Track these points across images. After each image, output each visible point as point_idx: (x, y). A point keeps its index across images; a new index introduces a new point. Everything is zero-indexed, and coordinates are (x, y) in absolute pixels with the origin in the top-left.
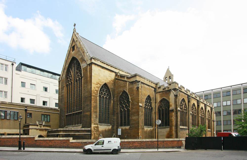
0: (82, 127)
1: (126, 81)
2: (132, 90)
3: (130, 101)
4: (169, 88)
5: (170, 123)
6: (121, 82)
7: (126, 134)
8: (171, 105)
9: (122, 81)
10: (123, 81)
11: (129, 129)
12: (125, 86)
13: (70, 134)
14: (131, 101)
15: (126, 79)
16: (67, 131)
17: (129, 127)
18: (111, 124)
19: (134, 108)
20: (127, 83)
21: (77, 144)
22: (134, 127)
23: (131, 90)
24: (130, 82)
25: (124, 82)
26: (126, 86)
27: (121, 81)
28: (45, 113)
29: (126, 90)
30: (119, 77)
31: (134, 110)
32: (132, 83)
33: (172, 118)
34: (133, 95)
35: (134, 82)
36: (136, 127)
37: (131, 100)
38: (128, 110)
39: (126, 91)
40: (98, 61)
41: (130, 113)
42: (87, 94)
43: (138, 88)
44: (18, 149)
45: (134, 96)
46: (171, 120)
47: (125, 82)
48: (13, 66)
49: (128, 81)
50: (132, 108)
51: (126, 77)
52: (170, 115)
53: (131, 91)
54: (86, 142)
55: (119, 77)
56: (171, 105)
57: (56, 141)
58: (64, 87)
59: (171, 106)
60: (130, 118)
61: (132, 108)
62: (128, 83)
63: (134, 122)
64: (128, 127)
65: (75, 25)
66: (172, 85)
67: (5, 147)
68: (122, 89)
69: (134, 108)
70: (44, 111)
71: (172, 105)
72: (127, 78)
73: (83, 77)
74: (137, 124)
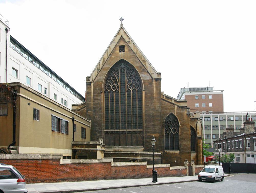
0: (144, 151)
1: (174, 104)
2: (181, 115)
3: (180, 125)
4: (194, 116)
5: (198, 149)
6: (168, 103)
7: (175, 159)
8: (199, 133)
9: (169, 103)
10: (170, 102)
11: (179, 153)
12: (173, 109)
13: (146, 159)
14: (181, 126)
15: (173, 102)
16: (144, 155)
17: (179, 151)
18: (143, 146)
19: (184, 133)
20: (175, 106)
21: (174, 172)
22: (185, 152)
23: (181, 115)
24: (178, 106)
25: (171, 104)
26: (174, 109)
27: (167, 103)
28: (83, 125)
29: (175, 113)
30: (165, 97)
31: (184, 135)
32: (182, 108)
33: (200, 145)
34: (183, 120)
35: (184, 108)
36: (187, 152)
37: (180, 125)
38: (178, 135)
39: (174, 114)
40: (148, 75)
41: (180, 137)
42: (153, 112)
43: (188, 115)
44: (152, 180)
45: (184, 121)
46: (199, 146)
47: (172, 105)
48: (7, 33)
49: (177, 105)
50: (182, 133)
51: (174, 100)
52: (198, 141)
53: (181, 115)
54: (180, 169)
55: (165, 97)
56: (199, 133)
57: (161, 169)
58: (102, 92)
59: (199, 134)
60: (180, 142)
61: (182, 133)
62: (176, 107)
63: (185, 147)
64: (177, 152)
65: (122, 19)
66: (197, 114)
67: (120, 179)
68: (169, 112)
69: (184, 133)
70: (83, 123)
71: (200, 133)
72: (174, 101)
73: (144, 90)
74: (188, 150)
